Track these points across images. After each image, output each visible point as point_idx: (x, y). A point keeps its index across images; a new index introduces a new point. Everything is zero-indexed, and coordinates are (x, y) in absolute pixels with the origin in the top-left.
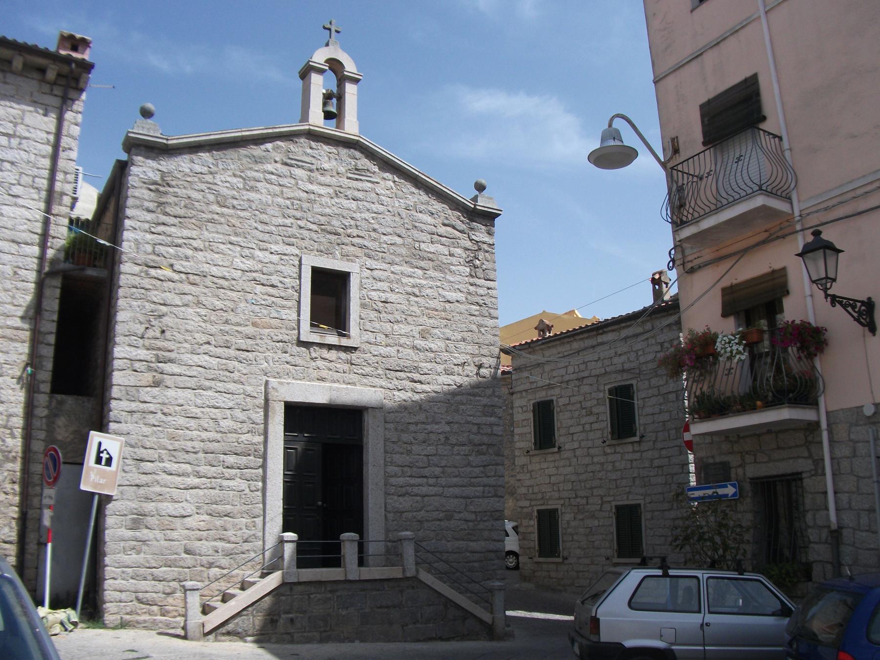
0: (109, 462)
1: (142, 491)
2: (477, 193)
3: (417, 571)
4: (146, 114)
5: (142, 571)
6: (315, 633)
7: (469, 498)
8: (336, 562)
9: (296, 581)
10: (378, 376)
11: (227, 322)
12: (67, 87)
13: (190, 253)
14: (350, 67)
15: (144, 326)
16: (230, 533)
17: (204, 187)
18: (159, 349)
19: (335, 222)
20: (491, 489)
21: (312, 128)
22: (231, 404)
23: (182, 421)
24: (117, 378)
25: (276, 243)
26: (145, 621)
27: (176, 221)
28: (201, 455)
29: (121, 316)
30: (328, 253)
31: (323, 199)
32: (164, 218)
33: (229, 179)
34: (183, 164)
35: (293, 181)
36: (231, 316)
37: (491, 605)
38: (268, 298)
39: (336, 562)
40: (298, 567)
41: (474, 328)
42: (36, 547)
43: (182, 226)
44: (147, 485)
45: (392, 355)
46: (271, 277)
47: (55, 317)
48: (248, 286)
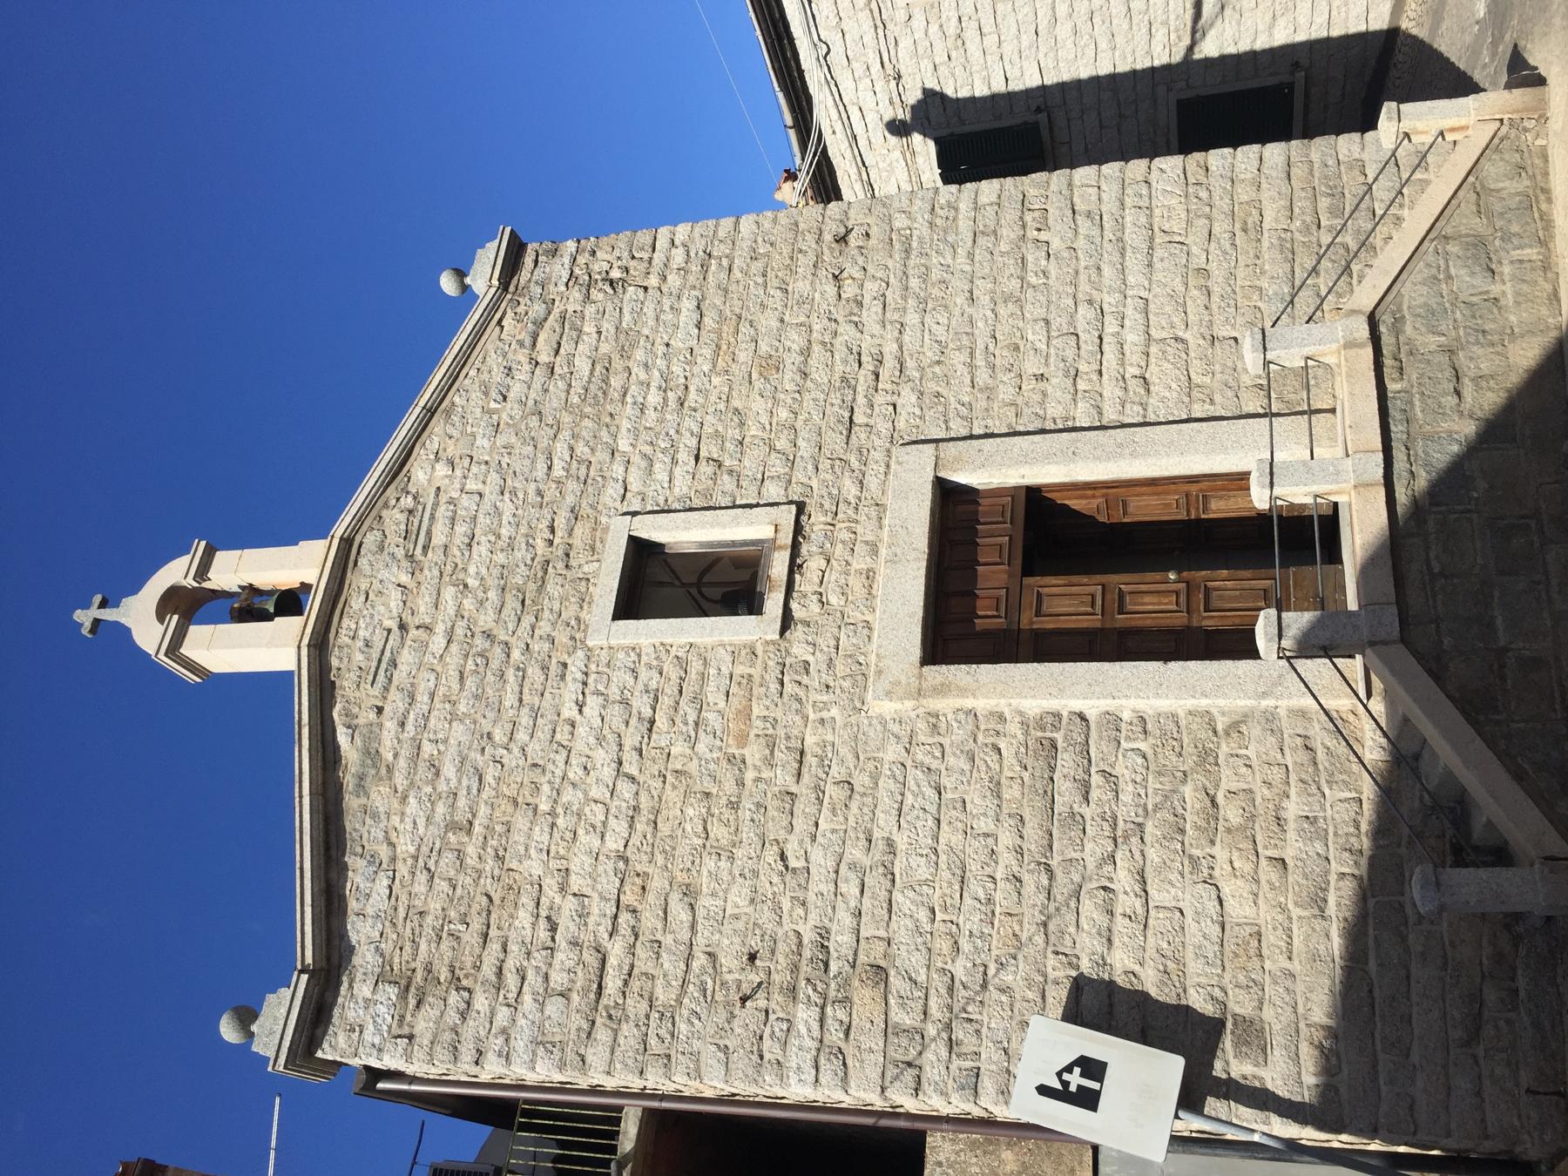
0: (1093, 1068)
3: (1353, 312)
7: (1152, 239)
20: (1129, 191)
21: (306, 641)
32: (488, 970)
34: (360, 931)
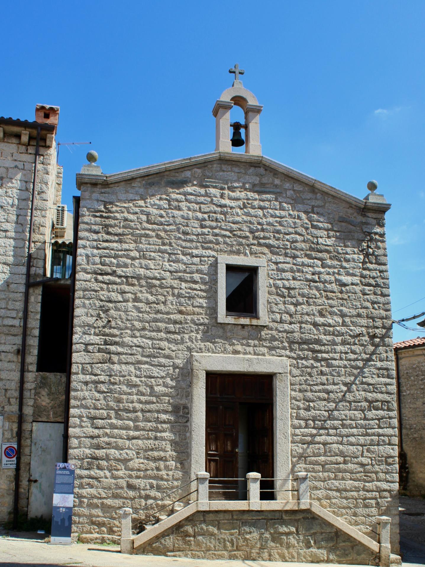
1: (95, 441)
2: (370, 192)
4: (91, 158)
5: (95, 501)
6: (225, 552)
8: (245, 496)
9: (208, 509)
10: (284, 348)
11: (158, 312)
12: (38, 146)
13: (129, 261)
14: (252, 101)
15: (95, 318)
16: (163, 473)
17: (137, 210)
18: (107, 335)
19: (245, 228)
22: (163, 374)
23: (124, 388)
24: (76, 357)
25: (197, 248)
26: (96, 539)
27: (117, 238)
28: (139, 414)
29: (77, 312)
30: (238, 253)
31: (234, 210)
33: (157, 202)
35: (209, 199)
36: (161, 307)
37: (379, 535)
38: (192, 291)
39: (245, 496)
40: (261, 499)
41: (369, 305)
42: (27, 483)
43: (120, 241)
44: (99, 436)
45: (296, 330)
46: (194, 275)
47: (38, 316)
48: (175, 283)
